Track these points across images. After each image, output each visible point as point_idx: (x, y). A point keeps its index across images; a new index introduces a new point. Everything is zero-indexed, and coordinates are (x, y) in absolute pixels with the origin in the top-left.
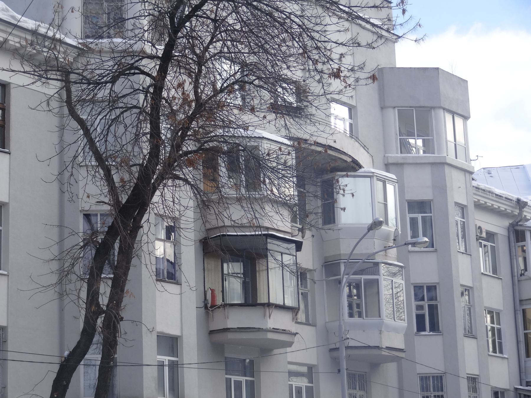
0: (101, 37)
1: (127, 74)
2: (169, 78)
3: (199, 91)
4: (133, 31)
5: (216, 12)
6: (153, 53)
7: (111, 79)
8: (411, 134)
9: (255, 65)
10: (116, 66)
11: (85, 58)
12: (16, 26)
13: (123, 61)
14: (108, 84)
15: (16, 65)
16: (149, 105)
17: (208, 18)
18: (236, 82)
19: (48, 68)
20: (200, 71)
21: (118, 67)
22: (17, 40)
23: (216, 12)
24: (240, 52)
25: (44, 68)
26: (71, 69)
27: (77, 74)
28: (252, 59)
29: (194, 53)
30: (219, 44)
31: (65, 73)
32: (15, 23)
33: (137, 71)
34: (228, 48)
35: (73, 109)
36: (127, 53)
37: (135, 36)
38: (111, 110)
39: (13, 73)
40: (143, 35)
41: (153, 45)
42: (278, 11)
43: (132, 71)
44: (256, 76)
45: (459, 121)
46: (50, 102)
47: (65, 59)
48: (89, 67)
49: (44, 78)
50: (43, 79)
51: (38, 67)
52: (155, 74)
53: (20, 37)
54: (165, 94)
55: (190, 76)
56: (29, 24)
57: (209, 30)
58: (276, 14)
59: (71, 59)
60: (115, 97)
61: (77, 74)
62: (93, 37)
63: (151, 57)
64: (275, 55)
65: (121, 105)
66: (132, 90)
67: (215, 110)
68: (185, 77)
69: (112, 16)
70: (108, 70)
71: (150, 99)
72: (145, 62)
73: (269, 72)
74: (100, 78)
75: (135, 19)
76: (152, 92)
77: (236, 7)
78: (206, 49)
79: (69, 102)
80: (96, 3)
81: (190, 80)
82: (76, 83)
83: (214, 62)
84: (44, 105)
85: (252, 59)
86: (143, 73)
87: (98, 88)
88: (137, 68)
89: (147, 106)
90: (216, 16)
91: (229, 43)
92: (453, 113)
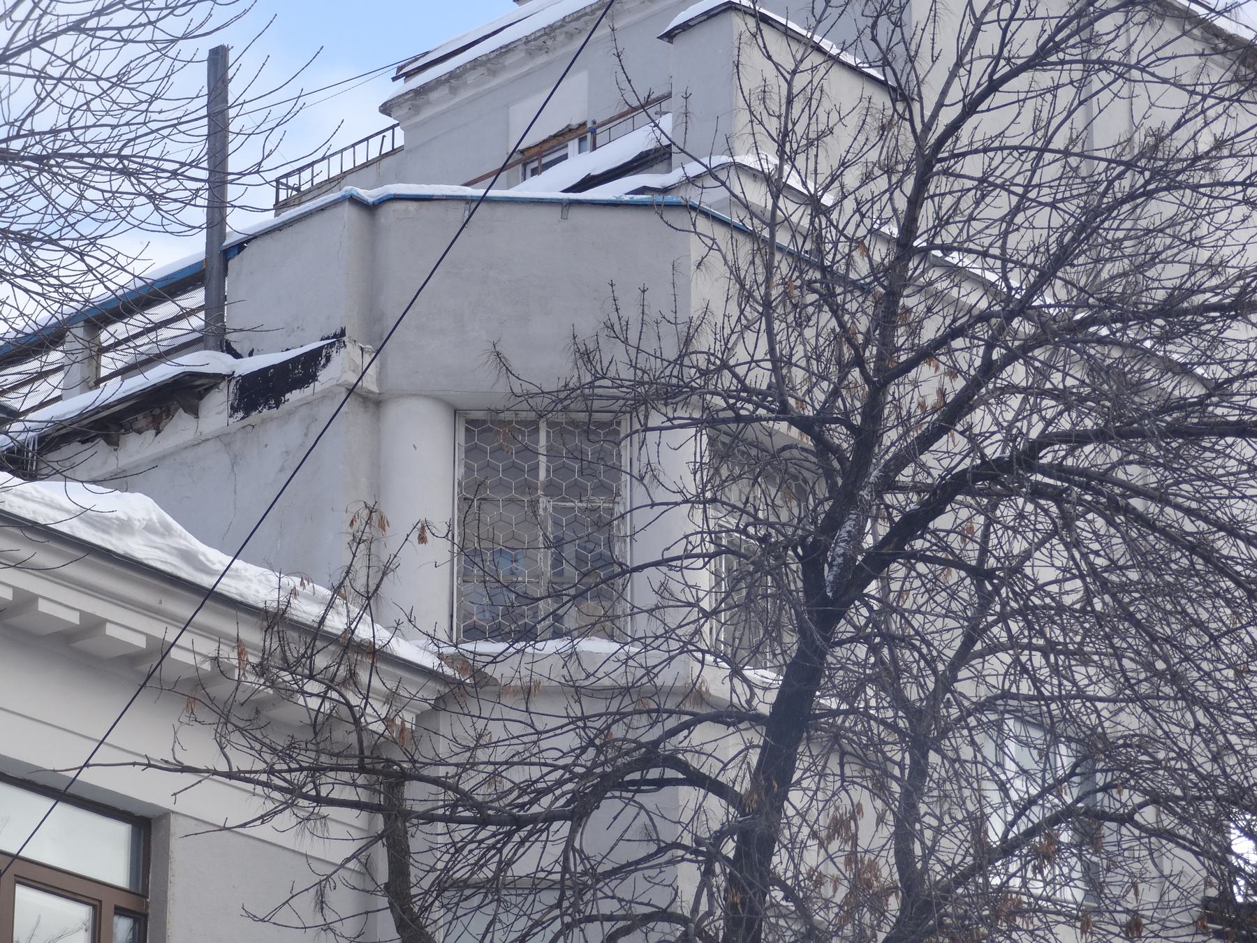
0: (529, 634)
1: (633, 782)
2: (796, 797)
3: (918, 850)
4: (657, 613)
5: (986, 536)
6: (735, 700)
7: (568, 803)
9: (1144, 743)
10: (591, 752)
11: (467, 721)
12: (210, 596)
13: (618, 731)
14: (556, 825)
15: (200, 748)
16: (719, 912)
17: (959, 563)
18: (1066, 815)
19: (324, 759)
20: (919, 770)
21: (597, 755)
22: (207, 647)
23: (986, 536)
24: (1081, 695)
25: (306, 759)
26: (413, 761)
27: (435, 781)
28: (1130, 721)
29: (900, 701)
30: (998, 663)
31: (385, 776)
32: (207, 581)
33: (670, 773)
34: (1035, 681)
35: (415, 919)
36: (638, 696)
37: (668, 634)
38: (568, 927)
39: (190, 778)
40: (698, 632)
41: (736, 672)
42: (1238, 536)
43: (654, 773)
44: (1145, 792)
46: (331, 896)
47: (388, 722)
48: (482, 755)
49: (306, 797)
50: (302, 802)
51: (285, 754)
52: (743, 786)
53: (219, 637)
54: (780, 862)
55: (879, 789)
56: (255, 583)
57: (955, 606)
58: (1225, 546)
59: (408, 718)
60: (584, 873)
61: (435, 781)
62: (496, 634)
63: (730, 716)
64: (1221, 707)
65: (607, 907)
66: (653, 848)
67: (983, 930)
68: (860, 795)
69: (569, 551)
70: (556, 768)
71: (720, 881)
72: (703, 733)
73: (1198, 774)
74: (526, 798)
75: (664, 569)
76: (731, 855)
77: (1068, 521)
78: (946, 682)
79: (398, 889)
80: (511, 500)
81: (879, 804)
82: (429, 818)
83: (980, 738)
84: (306, 903)
85: (1130, 721)
86: (696, 779)
87: (516, 838)
88: (672, 761)
89: (710, 913)
90: (984, 551)
91: (1038, 659)
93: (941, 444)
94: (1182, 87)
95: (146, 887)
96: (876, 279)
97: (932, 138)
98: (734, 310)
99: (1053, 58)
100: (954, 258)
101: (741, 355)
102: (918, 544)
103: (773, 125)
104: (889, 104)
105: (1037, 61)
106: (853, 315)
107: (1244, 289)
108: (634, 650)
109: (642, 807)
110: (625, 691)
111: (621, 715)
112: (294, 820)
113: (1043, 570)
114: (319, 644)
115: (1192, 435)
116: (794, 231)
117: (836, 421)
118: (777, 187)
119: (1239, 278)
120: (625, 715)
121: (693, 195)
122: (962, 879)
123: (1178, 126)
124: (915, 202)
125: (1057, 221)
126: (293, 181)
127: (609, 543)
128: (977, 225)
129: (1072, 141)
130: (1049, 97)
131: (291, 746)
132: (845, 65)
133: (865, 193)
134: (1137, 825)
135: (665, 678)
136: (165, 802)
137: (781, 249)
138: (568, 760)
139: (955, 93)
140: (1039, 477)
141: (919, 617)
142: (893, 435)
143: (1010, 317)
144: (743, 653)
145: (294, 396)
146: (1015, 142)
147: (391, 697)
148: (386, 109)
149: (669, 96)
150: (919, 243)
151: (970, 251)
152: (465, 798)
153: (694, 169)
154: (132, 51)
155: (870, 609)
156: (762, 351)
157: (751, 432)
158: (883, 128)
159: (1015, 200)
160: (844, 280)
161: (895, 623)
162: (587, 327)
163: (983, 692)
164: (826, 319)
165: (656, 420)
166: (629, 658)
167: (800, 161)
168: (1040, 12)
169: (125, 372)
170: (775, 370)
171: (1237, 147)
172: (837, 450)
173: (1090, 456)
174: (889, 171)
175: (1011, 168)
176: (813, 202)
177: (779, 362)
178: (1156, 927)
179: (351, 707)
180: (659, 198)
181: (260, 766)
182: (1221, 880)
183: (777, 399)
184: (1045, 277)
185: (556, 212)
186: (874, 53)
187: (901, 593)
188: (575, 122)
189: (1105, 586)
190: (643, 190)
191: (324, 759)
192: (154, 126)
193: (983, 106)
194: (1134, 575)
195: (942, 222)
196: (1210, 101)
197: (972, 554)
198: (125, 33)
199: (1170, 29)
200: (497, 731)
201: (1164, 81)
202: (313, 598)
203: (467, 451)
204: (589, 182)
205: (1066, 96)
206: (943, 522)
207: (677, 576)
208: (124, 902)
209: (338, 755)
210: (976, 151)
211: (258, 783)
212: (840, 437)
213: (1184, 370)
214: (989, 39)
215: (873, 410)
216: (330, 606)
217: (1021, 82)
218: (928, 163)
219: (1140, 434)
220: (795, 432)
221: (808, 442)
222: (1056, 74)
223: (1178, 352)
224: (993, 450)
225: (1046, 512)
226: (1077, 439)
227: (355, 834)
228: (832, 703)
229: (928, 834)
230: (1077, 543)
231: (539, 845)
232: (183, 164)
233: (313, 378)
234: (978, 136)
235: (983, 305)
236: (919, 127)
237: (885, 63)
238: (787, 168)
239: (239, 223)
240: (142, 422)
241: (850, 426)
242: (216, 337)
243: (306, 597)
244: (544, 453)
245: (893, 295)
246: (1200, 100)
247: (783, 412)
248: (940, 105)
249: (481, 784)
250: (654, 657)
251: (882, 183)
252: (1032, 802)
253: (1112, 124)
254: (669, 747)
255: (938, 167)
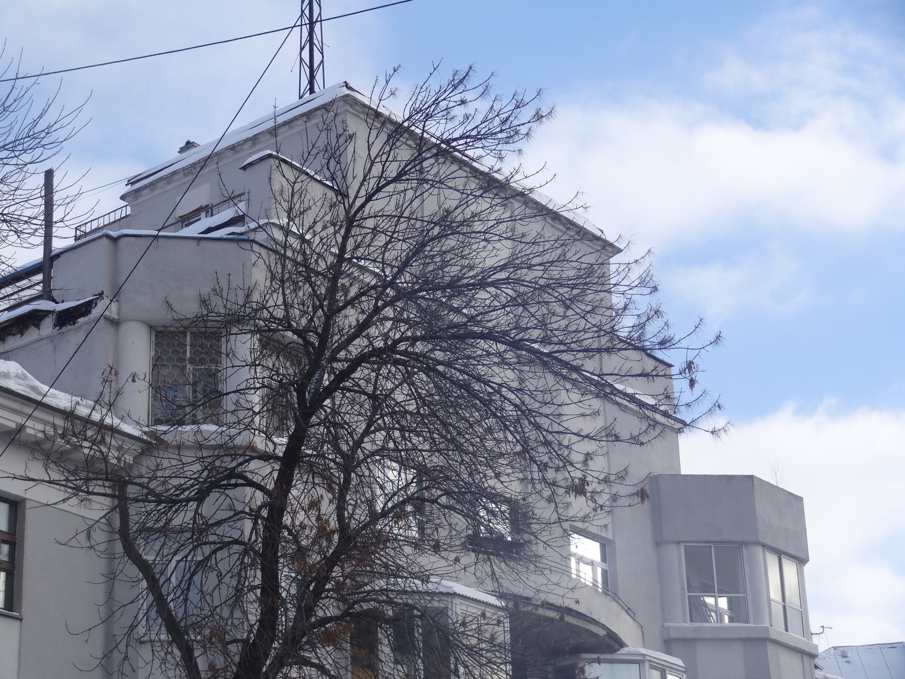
0: (181, 423)
1: (224, 485)
2: (294, 492)
5: (376, 381)
7: (196, 494)
8: (709, 590)
9: (442, 469)
10: (206, 473)
12: (39, 405)
13: (218, 463)
14: (191, 503)
15: (37, 470)
16: (260, 540)
17: (363, 392)
18: (409, 500)
19: (91, 475)
20: (348, 480)
22: (40, 427)
23: (376, 381)
25: (83, 475)
26: (129, 476)
28: (437, 460)
30: (380, 436)
31: (118, 482)
33: (240, 481)
36: (227, 449)
39: (32, 483)
40: (252, 420)
41: (269, 438)
43: (233, 481)
44: (441, 490)
45: (790, 568)
46: (93, 534)
47: (119, 459)
48: (159, 474)
49: (83, 491)
50: (81, 494)
52: (271, 486)
54: (287, 520)
55: (330, 489)
56: (61, 399)
57: (363, 411)
59: (129, 459)
60: (203, 524)
62: (167, 422)
63: (265, 457)
64: (474, 454)
65: (212, 538)
66: (232, 513)
68: (321, 491)
69: (199, 388)
70: (191, 479)
71: (261, 528)
72: (254, 465)
74: (178, 492)
76: (266, 516)
77: (410, 375)
78: (358, 444)
79: (124, 532)
82: (136, 500)
83: (372, 467)
84: (82, 537)
86: (250, 483)
87: (174, 509)
88: (241, 476)
89: (256, 541)
90: (375, 388)
92: (780, 554)
93: (357, 341)
94: (458, 191)
95: (15, 531)
96: (329, 271)
97: (353, 211)
98: (268, 283)
99: (404, 178)
100: (362, 263)
101: (271, 303)
102: (347, 384)
103: (286, 205)
104: (334, 196)
105: (397, 179)
106: (319, 287)
107: (483, 277)
108: (224, 429)
109: (228, 496)
110: (220, 446)
111: (219, 457)
112: (77, 501)
113: (399, 396)
114: (89, 426)
115: (462, 338)
116: (294, 251)
117: (312, 331)
118: (287, 232)
119: (481, 272)
120: (221, 456)
121: (252, 236)
122: (364, 528)
123: (456, 208)
124: (345, 238)
125: (405, 246)
126: (83, 228)
127: (216, 384)
128: (372, 249)
129: (412, 213)
130: (403, 195)
131: (75, 470)
132: (316, 180)
133: (324, 234)
134: (439, 504)
135: (238, 441)
136: (22, 494)
137: (288, 258)
138: (196, 476)
139: (363, 192)
140: (398, 356)
141: (348, 416)
142: (336, 338)
143: (385, 288)
144: (271, 430)
145: (81, 320)
146: (389, 213)
147: (120, 449)
148: (123, 198)
149: (244, 194)
150: (347, 256)
151: (368, 259)
152: (151, 492)
153: (253, 225)
154: (8, 169)
155: (326, 412)
156: (280, 301)
157: (276, 336)
158: (331, 206)
159: (388, 238)
160: (314, 271)
161: (338, 419)
162: (206, 290)
163: (375, 447)
164: (308, 288)
165: (234, 330)
166: (223, 431)
167: (297, 220)
168: (399, 158)
169: (9, 309)
170: (286, 310)
171: (482, 217)
172: (312, 344)
173: (420, 347)
174: (334, 225)
175: (384, 224)
176: (301, 238)
177: (287, 306)
178: (445, 547)
179: (102, 453)
180: (236, 237)
181: (63, 478)
182: (474, 526)
183: (286, 323)
184: (401, 271)
185: (194, 242)
186: (328, 174)
187: (340, 405)
188: (204, 204)
189: (424, 403)
190: (233, 233)
191: (91, 475)
192: (17, 201)
193: (374, 198)
194: (437, 398)
195: (357, 247)
196: (471, 197)
197: (370, 389)
198: (5, 161)
199: (455, 167)
200: (166, 464)
201: (451, 188)
202: (86, 406)
203: (156, 344)
204: (210, 230)
205: (410, 194)
206: (356, 375)
207: (243, 396)
208: (6, 538)
209: (97, 473)
210: (371, 217)
211: (62, 485)
212: (313, 339)
213: (458, 311)
214: (377, 170)
215: (327, 326)
216: (93, 409)
217: (390, 188)
218: (351, 221)
219: (439, 337)
220: (295, 337)
221: (300, 341)
222: (406, 185)
223: (456, 303)
224: (379, 344)
225: (400, 371)
226: (414, 340)
227: (105, 507)
228: (309, 452)
229: (350, 508)
230: (413, 384)
231: (183, 512)
232: (30, 218)
233: (90, 312)
234: (372, 211)
235: (373, 283)
236: (347, 206)
237: (333, 179)
238: (291, 223)
239: (58, 244)
240: (15, 330)
241: (316, 333)
242: (47, 294)
243: (83, 405)
244: (189, 347)
245: (335, 279)
246: (466, 198)
247: (289, 328)
248: (356, 197)
249: (158, 486)
250: (233, 431)
251: (331, 230)
252: (394, 494)
253: (431, 206)
254: (240, 470)
255: (355, 223)
